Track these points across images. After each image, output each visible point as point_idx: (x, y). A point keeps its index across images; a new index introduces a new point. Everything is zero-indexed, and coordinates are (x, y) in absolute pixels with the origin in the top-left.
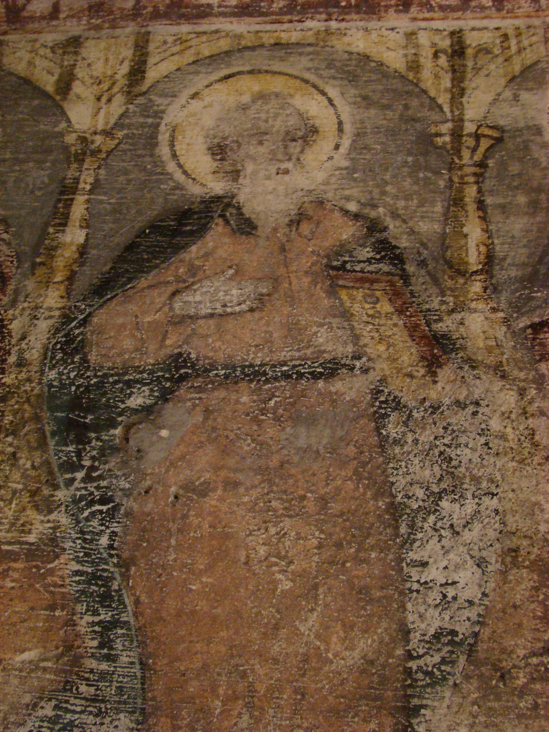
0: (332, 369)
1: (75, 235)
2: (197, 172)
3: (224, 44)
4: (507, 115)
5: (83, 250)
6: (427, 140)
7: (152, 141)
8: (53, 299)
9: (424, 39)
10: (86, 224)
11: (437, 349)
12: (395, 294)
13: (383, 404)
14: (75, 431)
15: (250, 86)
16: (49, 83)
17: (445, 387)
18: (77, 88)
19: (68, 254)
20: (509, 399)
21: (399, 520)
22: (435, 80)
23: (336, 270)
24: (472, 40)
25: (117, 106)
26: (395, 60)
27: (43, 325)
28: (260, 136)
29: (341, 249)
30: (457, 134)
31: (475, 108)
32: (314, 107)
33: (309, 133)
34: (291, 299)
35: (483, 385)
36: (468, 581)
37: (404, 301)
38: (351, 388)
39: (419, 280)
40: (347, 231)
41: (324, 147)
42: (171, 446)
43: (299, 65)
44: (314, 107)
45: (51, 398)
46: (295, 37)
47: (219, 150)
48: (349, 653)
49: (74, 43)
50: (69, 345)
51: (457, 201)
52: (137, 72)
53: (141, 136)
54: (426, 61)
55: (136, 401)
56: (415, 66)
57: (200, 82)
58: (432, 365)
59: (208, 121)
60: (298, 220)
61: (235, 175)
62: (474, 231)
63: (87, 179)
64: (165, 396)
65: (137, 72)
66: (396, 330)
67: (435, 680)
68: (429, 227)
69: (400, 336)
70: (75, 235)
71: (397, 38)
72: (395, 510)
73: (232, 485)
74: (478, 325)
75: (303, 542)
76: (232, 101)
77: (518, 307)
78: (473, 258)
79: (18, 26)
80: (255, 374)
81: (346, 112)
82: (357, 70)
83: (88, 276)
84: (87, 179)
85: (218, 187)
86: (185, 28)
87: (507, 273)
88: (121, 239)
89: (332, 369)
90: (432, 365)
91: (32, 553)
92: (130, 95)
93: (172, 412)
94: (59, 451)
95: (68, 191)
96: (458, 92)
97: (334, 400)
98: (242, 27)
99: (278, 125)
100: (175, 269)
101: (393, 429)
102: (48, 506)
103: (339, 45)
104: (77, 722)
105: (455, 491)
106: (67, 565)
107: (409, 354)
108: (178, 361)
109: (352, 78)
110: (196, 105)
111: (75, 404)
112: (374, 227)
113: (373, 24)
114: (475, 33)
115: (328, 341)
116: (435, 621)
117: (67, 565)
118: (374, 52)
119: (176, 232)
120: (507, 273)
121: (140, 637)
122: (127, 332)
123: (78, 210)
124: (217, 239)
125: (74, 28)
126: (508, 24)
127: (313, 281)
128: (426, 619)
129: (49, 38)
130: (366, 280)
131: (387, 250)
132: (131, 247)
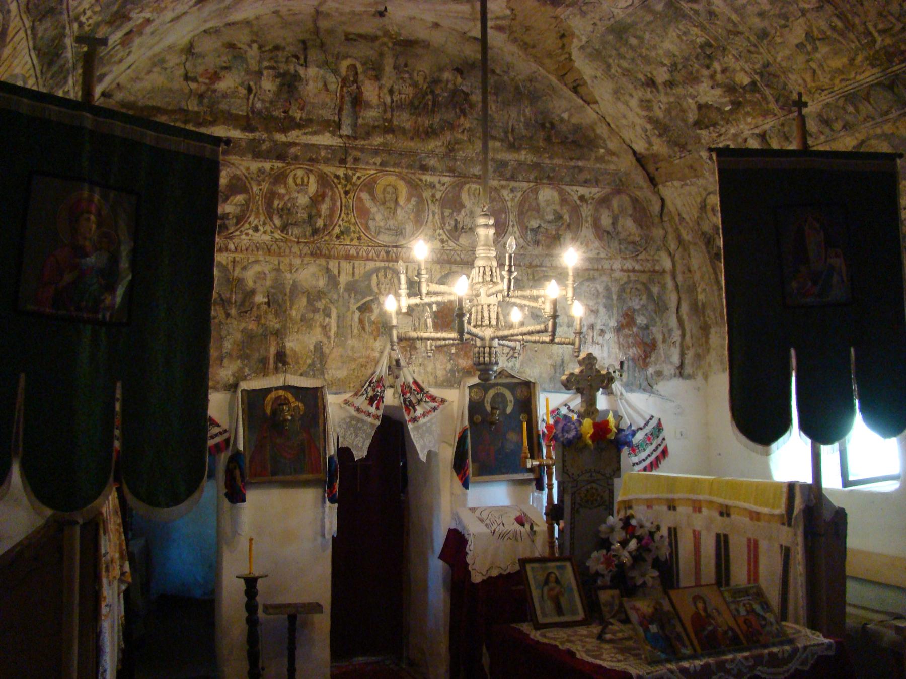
4: (240, 276)
6: (228, 279)
11: (228, 315)
22: (230, 267)
24: (237, 259)
26: (224, 262)
31: (236, 273)
35: (233, 321)
36: (229, 346)
37: (224, 308)
58: (227, 318)
74: (233, 312)
78: (233, 301)
79: (156, 60)
90: (227, 318)
96: (234, 270)
104: (704, 215)
107: (224, 316)
120: (238, 304)
127: (296, 81)
128: (224, 351)
130: (219, 304)
131: (222, 299)
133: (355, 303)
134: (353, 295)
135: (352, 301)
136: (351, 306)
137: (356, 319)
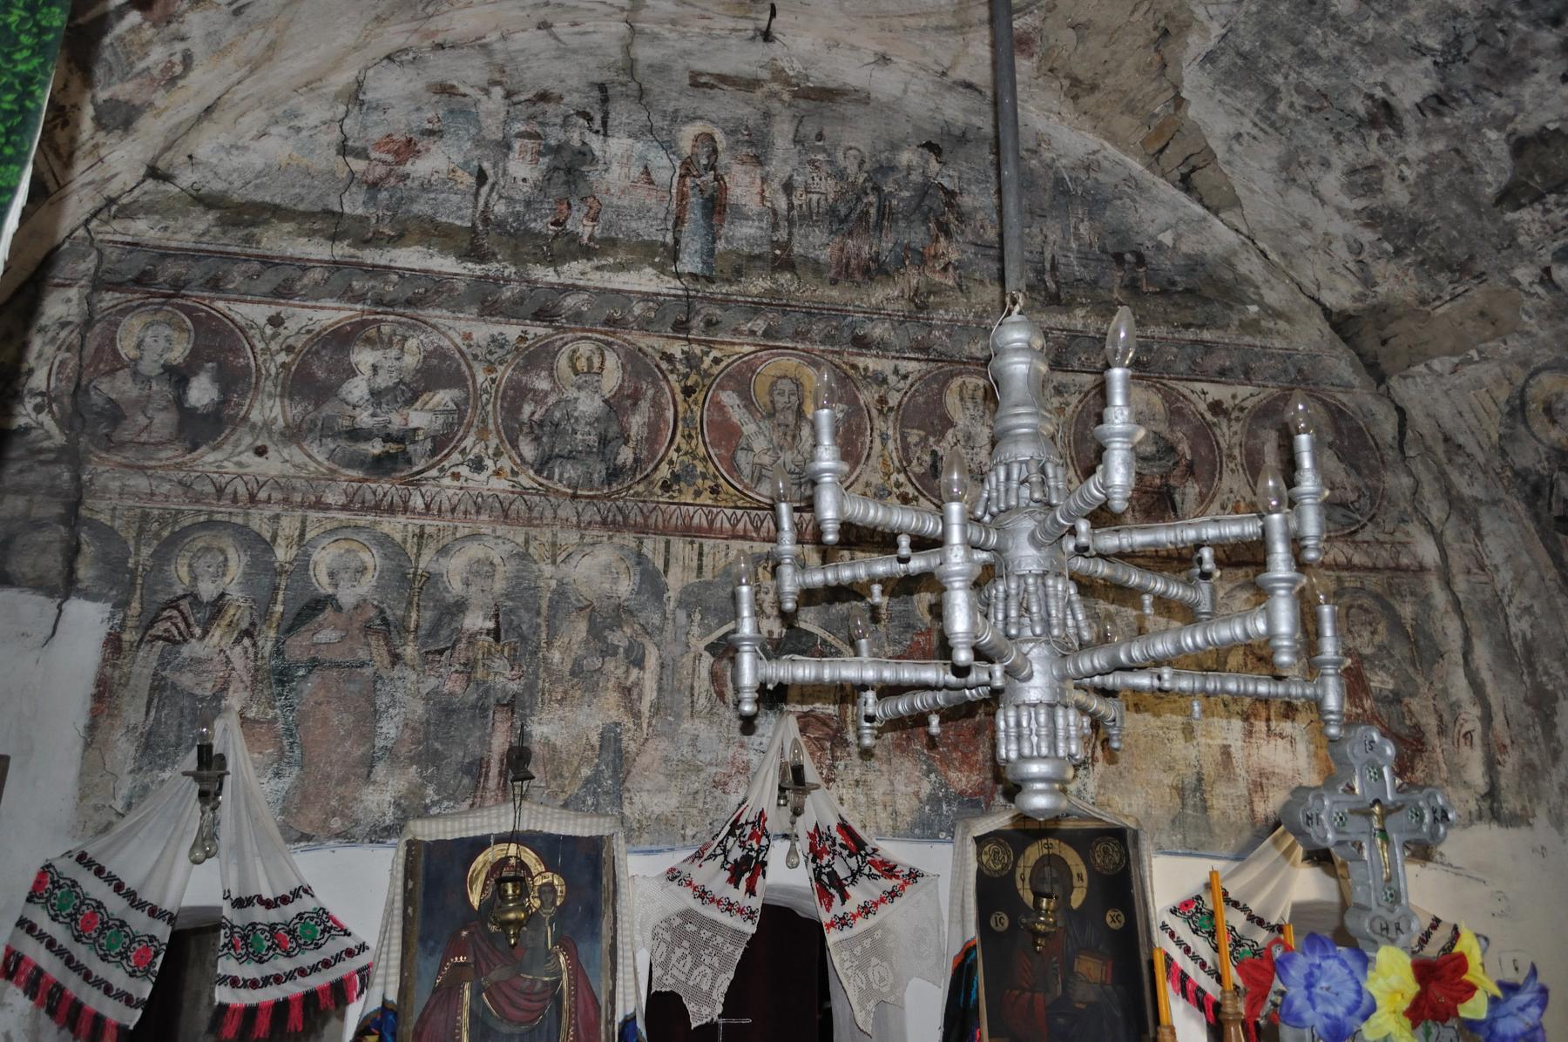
0: (362, 665)
1: (279, 608)
2: (323, 585)
3: (335, 524)
4: (433, 568)
5: (282, 614)
6: (404, 575)
7: (307, 569)
8: (272, 634)
9: (410, 528)
10: (284, 603)
11: (396, 658)
12: (385, 638)
13: (377, 677)
14: (281, 683)
15: (345, 545)
16: (268, 536)
17: (396, 673)
18: (279, 540)
19: (277, 615)
20: (414, 677)
21: (376, 714)
22: (411, 549)
23: (367, 628)
24: (428, 530)
25: (294, 551)
26: (398, 537)
27: (270, 644)
28: (346, 569)
29: (370, 620)
30: (415, 574)
32: (365, 556)
33: (362, 570)
34: (352, 638)
35: (408, 673)
38: (368, 671)
39: (394, 633)
40: (373, 613)
41: (368, 576)
42: (310, 688)
43: (363, 537)
44: (365, 556)
45: (273, 671)
46: (362, 523)
47: (331, 575)
48: (358, 752)
49: (277, 517)
50: (278, 652)
51: (410, 603)
52: (302, 535)
53: (303, 564)
54: (409, 540)
55: (301, 673)
56: (405, 541)
57: (325, 542)
58: (393, 664)
59: (328, 560)
60: (356, 608)
61: (336, 586)
62: (414, 615)
63: (283, 584)
64: (310, 672)
65: (302, 535)
66: (384, 651)
67: (380, 759)
68: (399, 613)
69: (385, 654)
70: (279, 608)
71: (400, 527)
72: (376, 711)
73: (329, 702)
74: (410, 651)
75: (349, 719)
76: (337, 552)
77: (423, 645)
78: (412, 626)
80: (338, 665)
81: (378, 560)
82: (384, 541)
83: (285, 625)
84: (283, 584)
85: (330, 591)
86: (321, 515)
87: (422, 632)
88: (295, 611)
89: (362, 665)
91: (269, 722)
92: (300, 546)
93: (313, 677)
94: (276, 689)
95: (276, 588)
96: (418, 555)
97: (361, 675)
98: (343, 516)
99: (353, 565)
100: (313, 624)
101: (379, 686)
102: (273, 708)
103: (378, 528)
105: (394, 706)
106: (280, 725)
107: (387, 660)
108: (314, 659)
109: (381, 545)
110: (324, 553)
111: (281, 673)
112: (382, 611)
113: (824, 78)
114: (663, 545)
115: (362, 654)
116: (382, 743)
117: (280, 725)
118: (390, 533)
119: (315, 609)
120: (422, 632)
121: (301, 746)
122: (298, 646)
123: (280, 597)
124: (328, 613)
125: (277, 509)
126: (441, 524)
128: (380, 743)
129: (268, 513)
131: (385, 621)
132: (299, 614)
133: (702, 636)
134: (697, 617)
135: (696, 630)
136: (693, 641)
137: (704, 672)
